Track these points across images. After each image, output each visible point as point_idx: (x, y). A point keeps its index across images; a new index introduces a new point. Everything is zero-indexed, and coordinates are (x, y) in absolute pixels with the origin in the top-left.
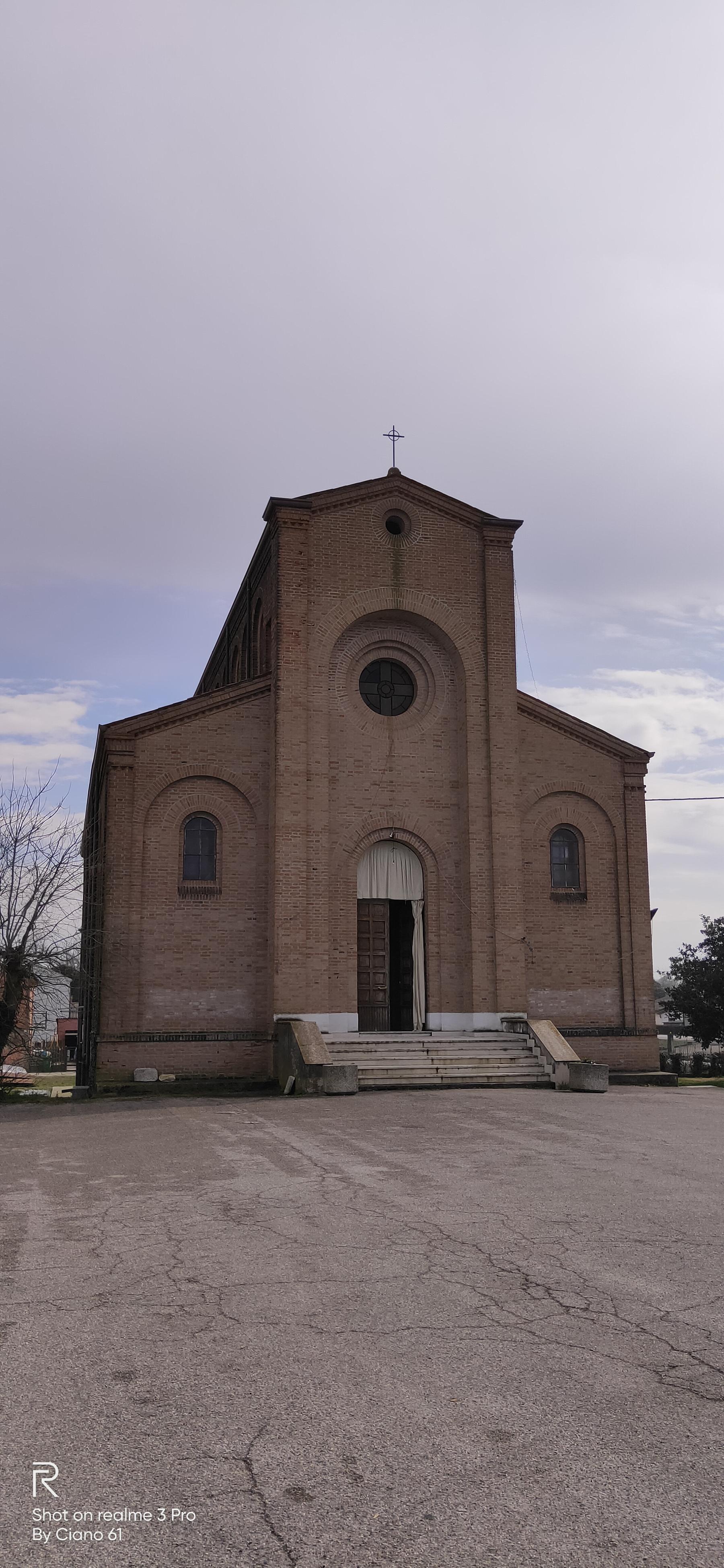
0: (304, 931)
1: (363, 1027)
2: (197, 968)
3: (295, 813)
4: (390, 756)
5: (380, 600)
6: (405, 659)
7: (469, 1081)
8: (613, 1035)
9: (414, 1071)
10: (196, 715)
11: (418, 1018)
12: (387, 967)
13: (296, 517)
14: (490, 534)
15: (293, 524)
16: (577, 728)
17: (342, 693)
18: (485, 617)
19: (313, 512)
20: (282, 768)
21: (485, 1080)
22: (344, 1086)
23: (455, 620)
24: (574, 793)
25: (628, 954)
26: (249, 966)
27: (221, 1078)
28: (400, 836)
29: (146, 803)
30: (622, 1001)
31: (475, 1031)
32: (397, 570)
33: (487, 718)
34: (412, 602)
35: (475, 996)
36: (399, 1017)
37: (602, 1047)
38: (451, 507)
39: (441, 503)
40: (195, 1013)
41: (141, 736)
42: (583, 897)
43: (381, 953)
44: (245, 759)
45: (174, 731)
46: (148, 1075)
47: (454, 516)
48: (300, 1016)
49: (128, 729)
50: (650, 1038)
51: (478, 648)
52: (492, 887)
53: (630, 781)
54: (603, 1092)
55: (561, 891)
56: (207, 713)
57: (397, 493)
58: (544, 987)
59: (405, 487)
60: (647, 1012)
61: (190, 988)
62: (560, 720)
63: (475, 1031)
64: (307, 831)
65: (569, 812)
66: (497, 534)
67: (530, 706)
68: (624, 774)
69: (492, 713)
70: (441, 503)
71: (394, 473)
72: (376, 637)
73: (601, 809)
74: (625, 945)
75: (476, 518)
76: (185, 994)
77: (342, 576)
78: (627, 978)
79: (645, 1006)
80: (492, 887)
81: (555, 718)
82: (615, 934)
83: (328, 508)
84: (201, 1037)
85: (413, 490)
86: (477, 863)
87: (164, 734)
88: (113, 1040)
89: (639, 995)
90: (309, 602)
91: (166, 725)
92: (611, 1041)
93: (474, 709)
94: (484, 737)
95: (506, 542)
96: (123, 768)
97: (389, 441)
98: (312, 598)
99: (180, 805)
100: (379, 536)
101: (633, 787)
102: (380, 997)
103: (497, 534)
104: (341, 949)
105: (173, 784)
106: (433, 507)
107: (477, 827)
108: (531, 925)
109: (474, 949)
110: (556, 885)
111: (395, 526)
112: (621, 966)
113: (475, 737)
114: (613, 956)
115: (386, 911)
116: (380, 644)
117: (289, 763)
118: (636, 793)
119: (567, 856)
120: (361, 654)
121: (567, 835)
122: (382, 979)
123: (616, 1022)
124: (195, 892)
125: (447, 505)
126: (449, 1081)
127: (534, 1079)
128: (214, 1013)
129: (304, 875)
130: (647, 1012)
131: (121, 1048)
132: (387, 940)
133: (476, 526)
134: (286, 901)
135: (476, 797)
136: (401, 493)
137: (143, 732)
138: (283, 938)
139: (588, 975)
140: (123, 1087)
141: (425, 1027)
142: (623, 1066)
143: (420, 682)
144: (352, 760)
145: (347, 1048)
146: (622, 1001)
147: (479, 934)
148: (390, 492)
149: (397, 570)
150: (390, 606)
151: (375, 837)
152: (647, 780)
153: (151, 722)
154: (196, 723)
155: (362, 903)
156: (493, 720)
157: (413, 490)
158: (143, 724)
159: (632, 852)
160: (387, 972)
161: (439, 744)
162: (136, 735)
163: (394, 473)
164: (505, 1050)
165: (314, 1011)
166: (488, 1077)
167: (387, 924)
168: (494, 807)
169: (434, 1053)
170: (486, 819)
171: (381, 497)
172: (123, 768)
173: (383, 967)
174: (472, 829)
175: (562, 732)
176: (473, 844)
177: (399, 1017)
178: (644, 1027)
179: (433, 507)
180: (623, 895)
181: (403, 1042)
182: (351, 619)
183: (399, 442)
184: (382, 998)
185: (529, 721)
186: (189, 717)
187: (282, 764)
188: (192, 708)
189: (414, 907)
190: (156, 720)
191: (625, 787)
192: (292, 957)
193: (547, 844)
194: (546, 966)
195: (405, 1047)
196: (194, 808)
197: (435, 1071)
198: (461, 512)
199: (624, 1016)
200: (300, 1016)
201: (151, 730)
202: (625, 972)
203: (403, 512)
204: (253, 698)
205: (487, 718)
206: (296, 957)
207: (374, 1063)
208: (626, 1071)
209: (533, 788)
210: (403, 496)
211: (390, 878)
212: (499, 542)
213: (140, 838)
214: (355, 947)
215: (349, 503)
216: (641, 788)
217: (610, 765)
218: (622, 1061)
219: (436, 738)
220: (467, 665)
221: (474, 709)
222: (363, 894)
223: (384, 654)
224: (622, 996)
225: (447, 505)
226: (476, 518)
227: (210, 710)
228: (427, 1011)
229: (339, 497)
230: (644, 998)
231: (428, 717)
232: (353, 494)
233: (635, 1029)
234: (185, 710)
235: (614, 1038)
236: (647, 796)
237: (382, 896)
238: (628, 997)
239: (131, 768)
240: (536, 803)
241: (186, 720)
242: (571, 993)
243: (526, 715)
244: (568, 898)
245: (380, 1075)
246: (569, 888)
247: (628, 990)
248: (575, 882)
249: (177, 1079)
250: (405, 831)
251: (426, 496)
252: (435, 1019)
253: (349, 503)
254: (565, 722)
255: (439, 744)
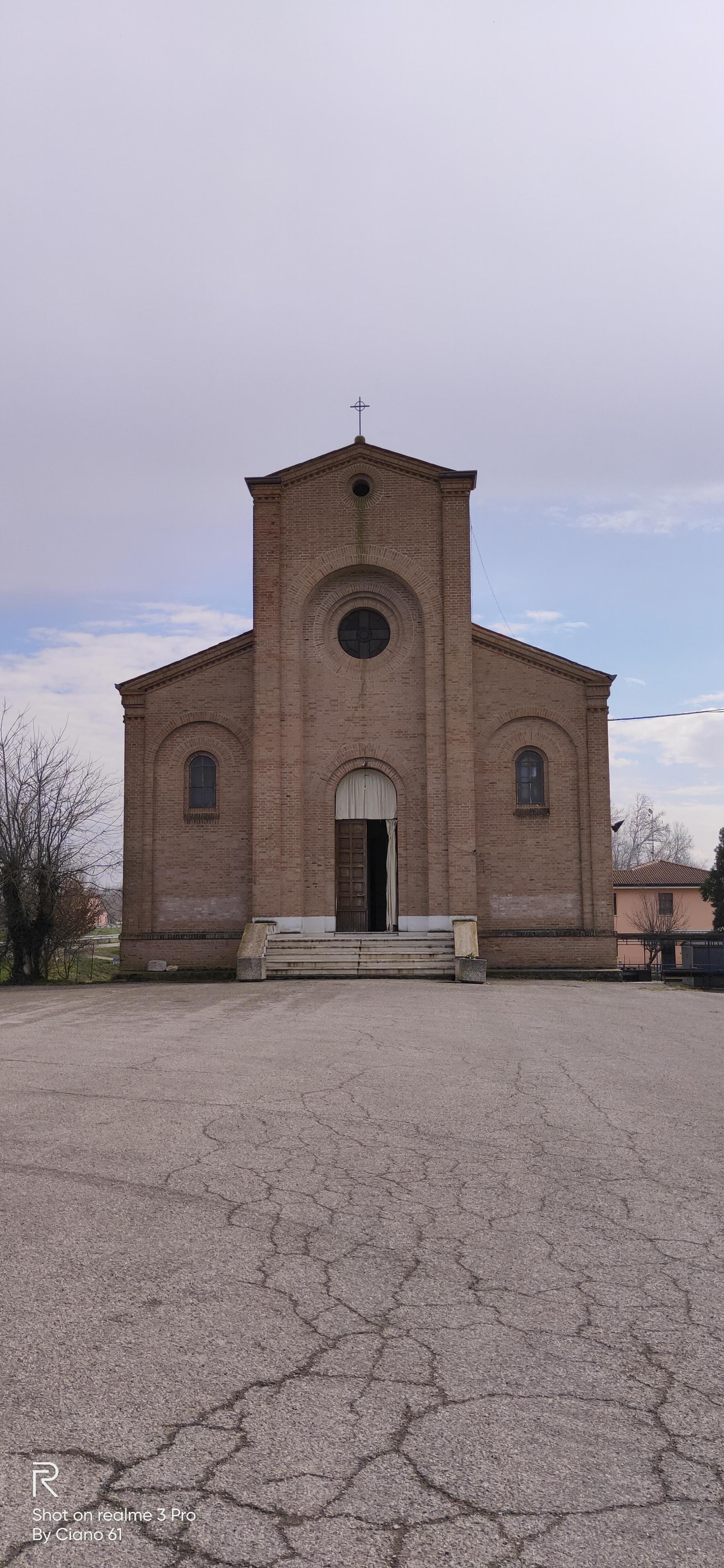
0: (279, 849)
1: (341, 927)
2: (200, 880)
3: (270, 749)
4: (362, 694)
5: (344, 557)
6: (378, 607)
7: (381, 972)
8: (570, 936)
9: (339, 964)
10: (195, 670)
11: (390, 921)
12: (365, 877)
13: (268, 492)
14: (448, 486)
15: (267, 498)
16: (539, 657)
17: (319, 642)
18: (442, 563)
19: (286, 485)
20: (258, 712)
21: (396, 972)
22: (250, 975)
23: (416, 570)
24: (538, 717)
25: (588, 863)
26: (243, 878)
27: (219, 969)
28: (371, 764)
29: (155, 747)
30: (582, 905)
31: (430, 932)
32: (361, 528)
33: (443, 655)
34: (375, 557)
35: (431, 902)
36: (376, 921)
37: (560, 946)
38: (410, 466)
39: (401, 463)
40: (199, 917)
41: (150, 691)
42: (546, 812)
43: (361, 866)
44: (236, 705)
45: (177, 685)
46: (159, 966)
47: (415, 474)
48: (275, 919)
49: (139, 686)
50: (608, 939)
51: (436, 592)
52: (446, 806)
53: (592, 703)
54: (481, 983)
55: (526, 807)
56: (204, 668)
57: (360, 459)
58: (507, 893)
59: (368, 452)
60: (605, 915)
61: (194, 896)
62: (522, 651)
63: (430, 932)
64: (281, 764)
65: (532, 735)
66: (454, 486)
67: (493, 640)
68: (587, 697)
69: (447, 650)
70: (401, 463)
71: (360, 441)
72: (350, 590)
73: (564, 731)
74: (585, 855)
75: (434, 473)
76: (191, 901)
77: (311, 540)
78: (586, 885)
79: (603, 910)
80: (446, 806)
81: (517, 650)
82: (577, 844)
83: (299, 480)
84: (202, 936)
85: (375, 455)
86: (434, 786)
87: (167, 688)
88: (132, 938)
89: (598, 900)
90: (282, 565)
91: (170, 680)
92: (568, 941)
93: (432, 647)
94: (441, 672)
95: (463, 492)
96: (136, 718)
97: (355, 412)
98: (285, 562)
99: (184, 746)
100: (345, 500)
101: (596, 709)
102: (359, 902)
103: (454, 486)
104: (319, 863)
105: (177, 729)
106: (395, 468)
107: (434, 752)
108: (495, 838)
109: (430, 861)
110: (521, 801)
111: (361, 489)
112: (581, 873)
113: (432, 673)
114: (574, 866)
115: (364, 829)
116: (355, 596)
117: (264, 707)
118: (598, 715)
119: (535, 775)
120: (337, 606)
121: (531, 757)
122: (361, 887)
123: (576, 924)
124: (197, 818)
125: (406, 465)
126: (364, 973)
127: (441, 972)
128: (213, 917)
129: (278, 801)
130: (605, 915)
131: (138, 944)
132: (365, 854)
133: (435, 481)
134: (263, 824)
135: (433, 727)
136: (364, 458)
137: (152, 687)
138: (260, 855)
139: (549, 882)
140: (131, 975)
141: (396, 928)
142: (579, 964)
143: (393, 627)
144: (328, 700)
145: (295, 944)
146: (582, 905)
147: (434, 848)
148: (355, 459)
149: (361, 528)
150: (354, 562)
151: (349, 767)
152: (610, 702)
153: (157, 678)
154: (195, 678)
155: (339, 824)
156: (449, 658)
157: (375, 455)
158: (150, 681)
159: (593, 769)
160: (365, 881)
161: (408, 681)
162: (146, 690)
163: (360, 441)
164: (430, 947)
165: (289, 914)
166: (399, 970)
167: (365, 841)
168: (449, 735)
169: (366, 949)
170: (443, 746)
171: (346, 464)
172: (136, 718)
173: (362, 878)
174: (430, 755)
175: (526, 662)
176: (430, 770)
177: (376, 921)
178: (601, 928)
179: (395, 468)
180: (584, 808)
181: (343, 940)
182: (319, 577)
183: (365, 411)
184: (362, 903)
185: (493, 654)
186: (189, 672)
187: (258, 708)
188: (189, 665)
189: (388, 825)
190: (161, 676)
191: (588, 709)
192: (268, 870)
193: (512, 765)
194: (508, 874)
195: (345, 944)
196: (195, 748)
197: (357, 964)
198: (420, 469)
199: (583, 919)
200: (275, 919)
201: (158, 685)
202: (584, 879)
203: (367, 476)
204: (242, 652)
205: (443, 655)
206: (271, 870)
207: (309, 957)
208: (583, 968)
209: (497, 715)
210: (366, 461)
211: (367, 801)
212: (456, 492)
213: (151, 775)
214: (333, 861)
215: (317, 473)
216: (605, 709)
217: (572, 689)
218: (579, 959)
219: (404, 676)
220: (426, 609)
221: (432, 647)
222: (342, 815)
223: (359, 604)
224: (582, 901)
225: (406, 465)
226: (434, 473)
227: (207, 665)
228: (397, 915)
229: (308, 470)
230: (603, 902)
231: (396, 658)
232: (319, 466)
233: (153, 932)
234: (184, 667)
235: (572, 938)
236: (609, 717)
237: (361, 817)
238: (587, 902)
239: (143, 718)
240: (500, 728)
241: (187, 675)
242: (532, 898)
243: (490, 649)
244: (532, 813)
245: (310, 966)
246: (533, 803)
247: (587, 895)
248: (541, 798)
249: (178, 970)
250: (377, 760)
251: (387, 459)
252: (404, 922)
253: (317, 473)
254: (527, 653)
255: (408, 681)
